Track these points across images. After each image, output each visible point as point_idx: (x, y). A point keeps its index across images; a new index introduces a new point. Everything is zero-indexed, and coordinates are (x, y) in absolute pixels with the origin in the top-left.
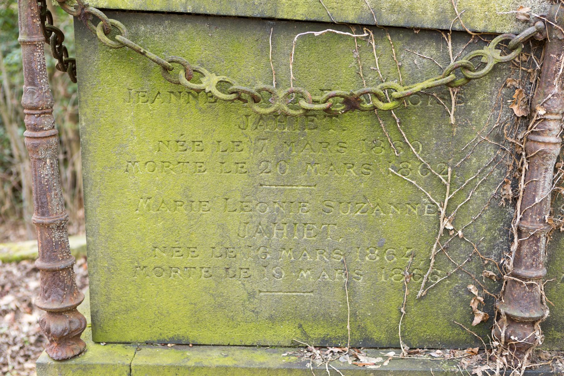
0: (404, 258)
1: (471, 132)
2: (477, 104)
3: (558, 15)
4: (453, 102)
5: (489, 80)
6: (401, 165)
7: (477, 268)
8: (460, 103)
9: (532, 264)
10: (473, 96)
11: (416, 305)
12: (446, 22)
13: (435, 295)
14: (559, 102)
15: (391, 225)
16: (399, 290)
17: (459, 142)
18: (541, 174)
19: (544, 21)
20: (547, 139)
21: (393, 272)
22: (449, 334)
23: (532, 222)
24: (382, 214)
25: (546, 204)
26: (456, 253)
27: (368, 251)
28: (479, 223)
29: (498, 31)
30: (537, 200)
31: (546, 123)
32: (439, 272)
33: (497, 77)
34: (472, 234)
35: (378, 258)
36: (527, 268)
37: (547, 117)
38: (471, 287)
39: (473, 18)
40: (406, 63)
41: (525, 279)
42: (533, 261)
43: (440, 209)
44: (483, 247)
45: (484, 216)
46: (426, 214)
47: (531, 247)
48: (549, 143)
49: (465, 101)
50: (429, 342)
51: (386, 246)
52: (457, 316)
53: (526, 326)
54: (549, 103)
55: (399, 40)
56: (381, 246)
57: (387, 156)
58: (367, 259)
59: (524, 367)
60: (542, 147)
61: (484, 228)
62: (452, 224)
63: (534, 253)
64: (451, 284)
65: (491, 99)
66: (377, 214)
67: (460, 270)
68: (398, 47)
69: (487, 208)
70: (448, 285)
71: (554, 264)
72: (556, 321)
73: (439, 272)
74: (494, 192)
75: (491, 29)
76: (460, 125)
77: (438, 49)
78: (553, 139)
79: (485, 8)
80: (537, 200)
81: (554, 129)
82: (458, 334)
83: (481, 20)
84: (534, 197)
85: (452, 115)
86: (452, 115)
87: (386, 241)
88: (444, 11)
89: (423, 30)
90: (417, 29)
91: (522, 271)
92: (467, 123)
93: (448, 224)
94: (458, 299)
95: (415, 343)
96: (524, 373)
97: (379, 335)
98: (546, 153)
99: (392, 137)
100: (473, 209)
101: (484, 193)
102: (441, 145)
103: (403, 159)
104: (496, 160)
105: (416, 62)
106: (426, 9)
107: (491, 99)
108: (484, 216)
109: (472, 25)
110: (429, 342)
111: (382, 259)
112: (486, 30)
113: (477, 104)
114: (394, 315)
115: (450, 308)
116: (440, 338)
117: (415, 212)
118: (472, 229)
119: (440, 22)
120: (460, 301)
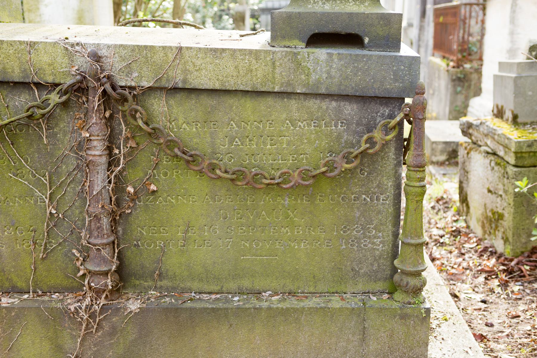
0: (29, 232)
1: (59, 149)
2: (60, 130)
3: (89, 71)
4: (44, 129)
5: (66, 114)
6: (18, 172)
7: (77, 238)
8: (49, 130)
9: (98, 235)
10: (57, 125)
11: (41, 264)
12: (28, 77)
13: (53, 256)
14: (97, 128)
15: (18, 211)
16: (29, 254)
17: (52, 155)
18: (95, 176)
19: (82, 75)
20: (93, 153)
21: (24, 242)
22: (66, 283)
23: (94, 207)
24: (11, 204)
25: (101, 195)
26: (62, 228)
27: (6, 229)
28: (74, 208)
29: (62, 82)
30: (95, 193)
31: (92, 142)
32: (53, 241)
33: (70, 112)
34: (70, 216)
35: (13, 233)
36: (95, 238)
37: (91, 138)
38: (74, 251)
39: (44, 74)
40: (11, 104)
41: (94, 245)
42: (99, 233)
43: (45, 200)
44: (78, 224)
45: (76, 204)
46: (39, 203)
47: (96, 224)
48: (94, 155)
49: (53, 128)
50: (54, 288)
51: (17, 225)
52: (70, 270)
53: (101, 277)
54: (91, 129)
55: (4, 90)
56: (13, 225)
57: (8, 166)
58: (6, 233)
59: (101, 304)
60: (91, 158)
61: (77, 212)
62: (56, 210)
63: (98, 228)
64: (62, 249)
65: (68, 127)
66: (7, 204)
67: (65, 241)
68: (4, 94)
69: (77, 198)
70: (60, 250)
71: (127, 235)
72: (134, 273)
73: (53, 241)
74: (80, 188)
75: (57, 81)
76: (51, 144)
77: (30, 95)
78: (97, 153)
79: (52, 67)
80: (95, 193)
81: (97, 146)
82: (72, 283)
83: (50, 75)
84: (93, 191)
85: (44, 138)
86: (44, 138)
87: (16, 222)
88: (25, 70)
89: (15, 83)
90: (12, 82)
91: (92, 240)
92: (56, 143)
93: (53, 209)
94: (68, 259)
95: (45, 289)
96: (101, 308)
97: (20, 284)
98: (93, 162)
99: (9, 153)
100: (68, 199)
101: (74, 189)
102: (41, 157)
103: (18, 168)
104: (78, 166)
105: (17, 103)
106: (14, 70)
107: (68, 127)
108: (76, 204)
109: (45, 78)
110: (54, 288)
111: (15, 233)
112: (54, 82)
113: (60, 130)
114: (28, 271)
115: (64, 265)
116: (60, 285)
117: (32, 202)
118: (69, 213)
119: (24, 78)
120: (69, 261)
